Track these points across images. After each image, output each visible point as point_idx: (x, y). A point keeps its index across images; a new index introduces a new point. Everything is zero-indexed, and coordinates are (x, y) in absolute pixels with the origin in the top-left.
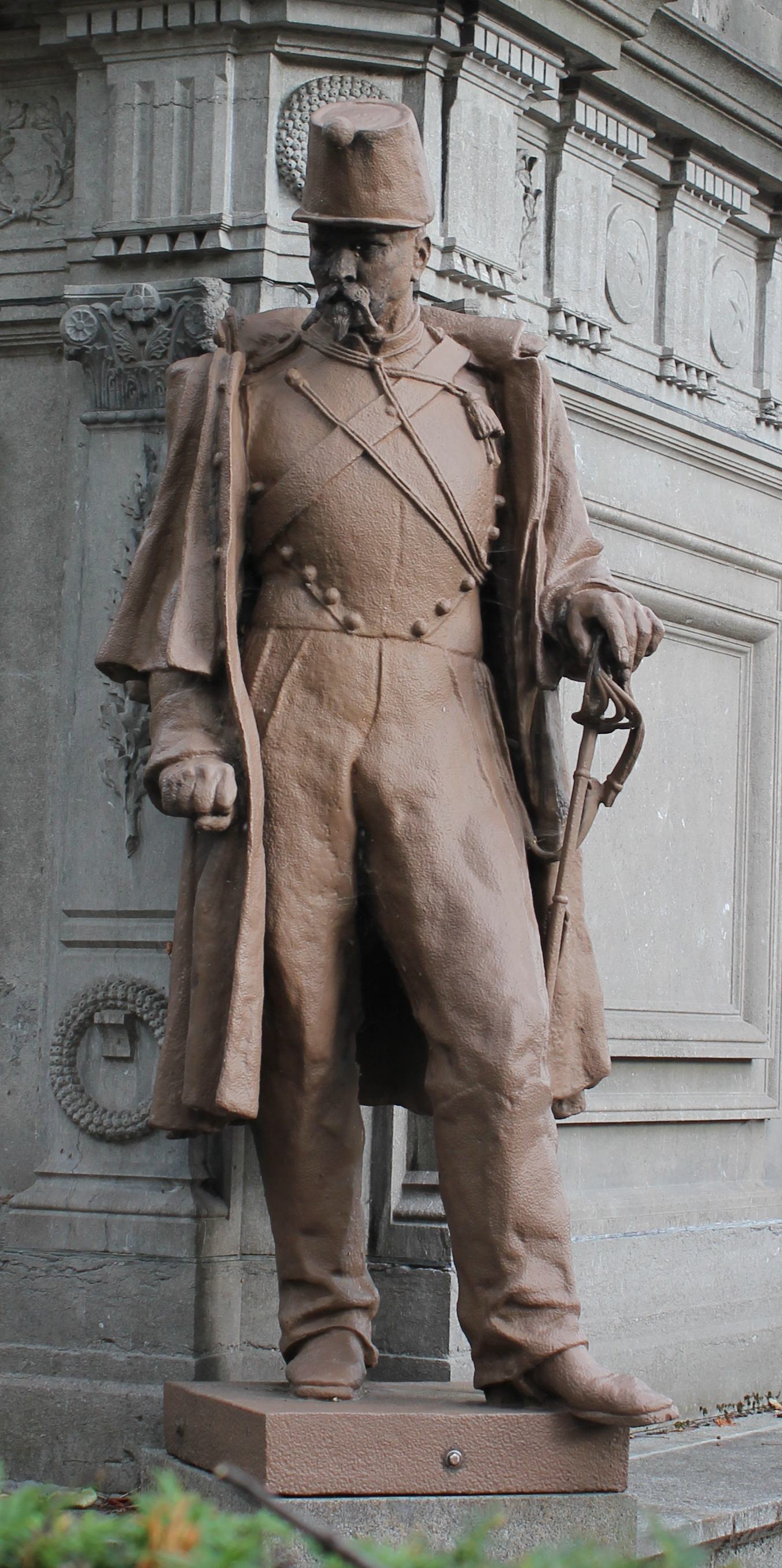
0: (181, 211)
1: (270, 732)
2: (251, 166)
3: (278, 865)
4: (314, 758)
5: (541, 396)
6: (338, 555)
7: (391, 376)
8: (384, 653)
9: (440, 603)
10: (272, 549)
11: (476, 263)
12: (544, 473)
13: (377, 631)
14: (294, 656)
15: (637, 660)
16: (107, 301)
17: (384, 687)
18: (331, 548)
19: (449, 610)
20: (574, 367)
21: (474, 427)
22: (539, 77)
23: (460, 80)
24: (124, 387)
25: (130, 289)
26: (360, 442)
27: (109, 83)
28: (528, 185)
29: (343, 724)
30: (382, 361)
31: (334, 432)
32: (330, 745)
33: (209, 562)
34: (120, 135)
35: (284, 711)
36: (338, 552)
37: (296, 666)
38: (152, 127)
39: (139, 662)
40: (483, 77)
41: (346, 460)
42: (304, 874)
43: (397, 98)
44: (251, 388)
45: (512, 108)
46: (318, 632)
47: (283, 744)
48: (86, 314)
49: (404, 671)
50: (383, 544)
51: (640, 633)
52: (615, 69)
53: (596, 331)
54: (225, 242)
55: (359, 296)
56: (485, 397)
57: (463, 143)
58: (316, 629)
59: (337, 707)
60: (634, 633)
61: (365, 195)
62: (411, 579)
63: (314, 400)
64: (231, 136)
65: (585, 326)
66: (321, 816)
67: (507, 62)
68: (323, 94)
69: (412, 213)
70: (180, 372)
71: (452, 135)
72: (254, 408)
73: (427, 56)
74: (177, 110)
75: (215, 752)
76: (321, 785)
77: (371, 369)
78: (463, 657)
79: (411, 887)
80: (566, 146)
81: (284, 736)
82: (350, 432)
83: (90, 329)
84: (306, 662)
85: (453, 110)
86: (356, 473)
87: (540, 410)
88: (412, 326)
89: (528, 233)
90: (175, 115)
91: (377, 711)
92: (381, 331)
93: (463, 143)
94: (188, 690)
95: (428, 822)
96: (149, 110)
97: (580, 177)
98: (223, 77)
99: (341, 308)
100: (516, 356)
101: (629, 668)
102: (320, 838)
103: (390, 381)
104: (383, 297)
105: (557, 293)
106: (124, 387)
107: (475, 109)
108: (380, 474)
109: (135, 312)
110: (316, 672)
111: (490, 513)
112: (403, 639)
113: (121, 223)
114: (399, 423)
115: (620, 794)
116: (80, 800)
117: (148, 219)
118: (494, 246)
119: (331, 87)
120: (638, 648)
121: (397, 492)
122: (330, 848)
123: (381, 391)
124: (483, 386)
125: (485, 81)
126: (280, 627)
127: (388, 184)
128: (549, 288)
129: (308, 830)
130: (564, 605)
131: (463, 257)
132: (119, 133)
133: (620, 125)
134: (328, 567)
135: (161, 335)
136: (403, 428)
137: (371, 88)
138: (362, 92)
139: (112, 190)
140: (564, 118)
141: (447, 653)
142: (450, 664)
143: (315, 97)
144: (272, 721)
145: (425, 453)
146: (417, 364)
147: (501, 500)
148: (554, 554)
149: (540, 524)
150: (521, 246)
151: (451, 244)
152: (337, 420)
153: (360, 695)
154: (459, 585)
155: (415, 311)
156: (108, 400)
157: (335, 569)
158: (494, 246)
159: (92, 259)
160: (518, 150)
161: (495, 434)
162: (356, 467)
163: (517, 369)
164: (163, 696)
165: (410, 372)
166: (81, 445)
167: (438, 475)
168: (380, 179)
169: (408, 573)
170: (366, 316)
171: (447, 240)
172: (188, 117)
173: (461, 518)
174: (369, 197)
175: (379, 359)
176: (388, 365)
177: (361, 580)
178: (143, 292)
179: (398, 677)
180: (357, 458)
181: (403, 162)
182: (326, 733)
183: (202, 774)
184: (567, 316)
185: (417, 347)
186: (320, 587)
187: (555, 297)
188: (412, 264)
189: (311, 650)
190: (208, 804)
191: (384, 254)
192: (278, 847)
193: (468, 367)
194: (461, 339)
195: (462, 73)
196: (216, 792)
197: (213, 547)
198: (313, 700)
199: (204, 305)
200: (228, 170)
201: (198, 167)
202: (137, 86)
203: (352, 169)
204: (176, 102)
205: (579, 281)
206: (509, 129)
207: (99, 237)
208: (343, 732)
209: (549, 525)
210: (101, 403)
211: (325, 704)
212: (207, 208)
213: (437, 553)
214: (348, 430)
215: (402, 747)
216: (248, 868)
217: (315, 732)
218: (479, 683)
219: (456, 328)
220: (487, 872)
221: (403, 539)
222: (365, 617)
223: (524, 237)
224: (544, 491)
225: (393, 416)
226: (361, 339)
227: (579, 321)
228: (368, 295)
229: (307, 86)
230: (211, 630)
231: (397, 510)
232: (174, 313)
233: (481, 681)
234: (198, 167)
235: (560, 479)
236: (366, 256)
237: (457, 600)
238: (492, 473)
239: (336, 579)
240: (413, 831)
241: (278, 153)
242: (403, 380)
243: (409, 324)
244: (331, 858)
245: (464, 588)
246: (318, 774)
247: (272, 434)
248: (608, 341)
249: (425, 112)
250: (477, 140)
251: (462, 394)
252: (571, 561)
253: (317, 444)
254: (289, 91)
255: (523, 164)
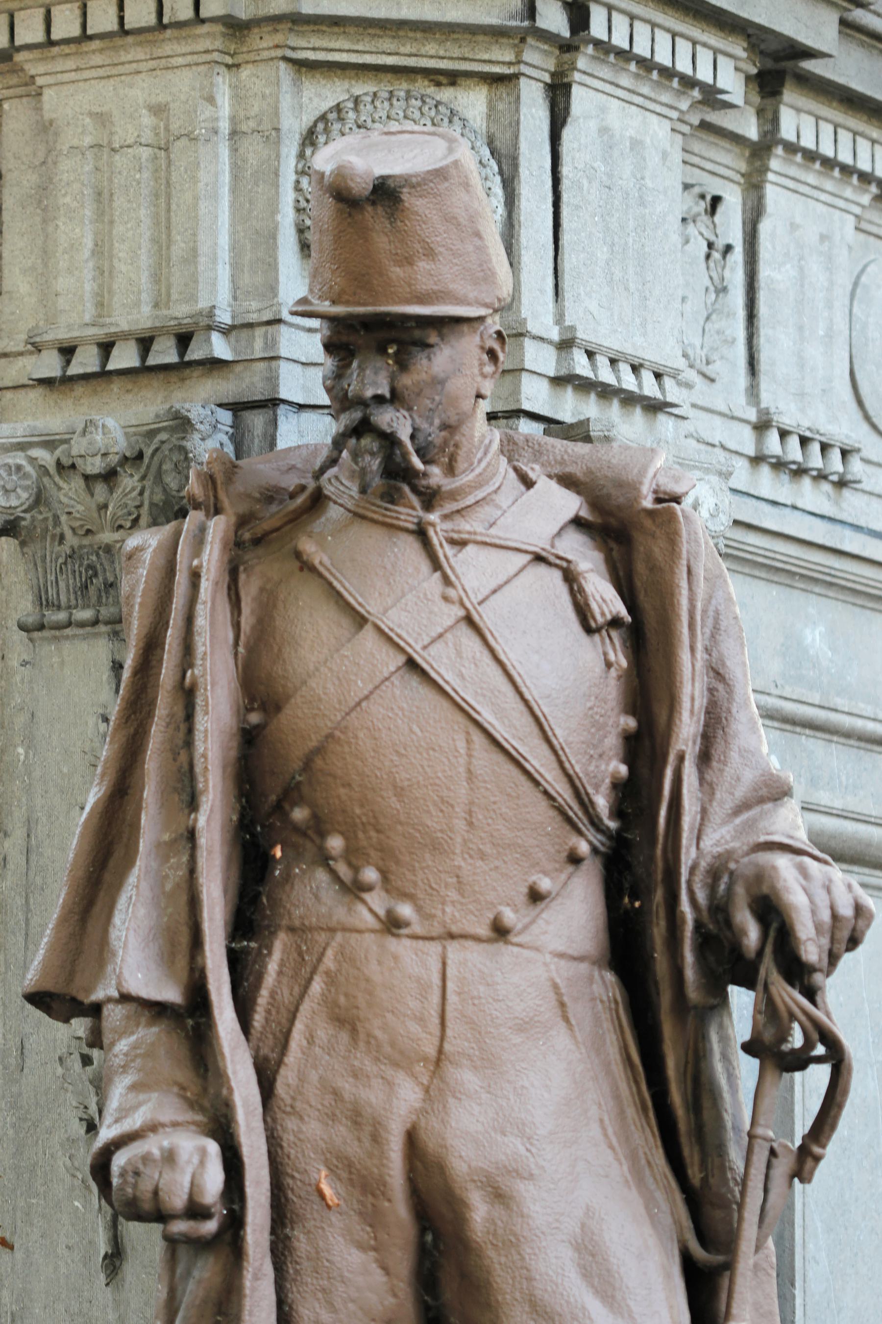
0: (156, 305)
1: (280, 1089)
2: (257, 232)
3: (299, 1292)
4: (347, 1126)
5: (684, 562)
6: (375, 817)
7: (452, 542)
8: (449, 962)
9: (535, 883)
10: (280, 809)
11: (613, 362)
12: (693, 679)
13: (437, 930)
14: (314, 972)
15: (833, 959)
16: (50, 445)
17: (450, 1014)
18: (362, 806)
19: (549, 893)
20: (804, 511)
21: (582, 612)
22: (704, 74)
23: (576, 90)
24: (80, 573)
25: (80, 428)
26: (402, 644)
27: (47, 116)
28: (712, 238)
29: (389, 1072)
30: (438, 521)
31: (364, 631)
32: (371, 1106)
33: (182, 835)
34: (65, 195)
35: (300, 1055)
36: (372, 811)
37: (317, 986)
38: (110, 180)
39: (89, 990)
40: (613, 80)
41: (381, 672)
42: (338, 1303)
43: (478, 119)
44: (245, 570)
45: (667, 125)
46: (347, 935)
47: (299, 1105)
48: (19, 468)
49: (482, 988)
50: (442, 798)
51: (835, 917)
52: (830, 56)
53: (835, 455)
54: (220, 348)
55: (395, 425)
56: (603, 567)
57: (585, 182)
58: (345, 929)
59: (379, 1046)
60: (825, 916)
61: (397, 272)
62: (488, 849)
63: (336, 583)
64: (227, 189)
65: (816, 448)
66: (360, 1214)
67: (649, 57)
68: (363, 118)
69: (472, 295)
70: (139, 549)
71: (565, 170)
72: (249, 599)
73: (519, 54)
74: (145, 153)
75: (194, 1123)
76: (358, 1167)
77: (421, 533)
78: (574, 964)
79: (498, 1317)
80: (771, 176)
81: (301, 1093)
82: (387, 630)
83: (26, 488)
84: (331, 979)
85: (567, 134)
86: (398, 692)
87: (684, 584)
88: (483, 464)
89: (714, 311)
90: (143, 160)
91: (440, 1051)
92: (436, 475)
93: (585, 182)
94: (155, 1029)
95: (522, 1216)
96: (105, 157)
97: (798, 220)
98: (211, 100)
99: (367, 442)
100: (648, 503)
101: (821, 970)
102: (362, 1247)
103: (449, 550)
104: (431, 424)
105: (766, 399)
106: (80, 573)
107: (604, 130)
108: (434, 692)
109: (89, 460)
110: (346, 995)
111: (612, 742)
112: (477, 939)
113: (70, 327)
114: (462, 613)
115: (822, 1164)
116: (34, 1201)
117: (108, 320)
118: (645, 334)
119: (375, 107)
120: (833, 940)
121: (460, 718)
122: (377, 1261)
123: (436, 565)
124: (600, 550)
125: (617, 86)
126: (292, 929)
127: (430, 253)
128: (753, 392)
129: (343, 1236)
130: (725, 879)
131: (590, 354)
132: (63, 192)
133: (859, 139)
134: (361, 835)
135: (130, 492)
136: (469, 620)
137: (436, 106)
138: (422, 113)
139: (55, 278)
140: (764, 134)
141: (548, 957)
142: (554, 974)
143: (350, 123)
144: (283, 1071)
145: (503, 657)
146: (494, 523)
147: (631, 723)
148: (711, 801)
149: (687, 757)
150: (704, 330)
151: (569, 336)
152: (368, 612)
153: (414, 1028)
154: (565, 854)
155: (490, 442)
156: (58, 594)
157: (370, 838)
158: (645, 334)
159: (31, 382)
160: (687, 187)
161: (615, 622)
162: (397, 683)
163: (648, 523)
164: (119, 1039)
165: (481, 534)
166: (24, 664)
167: (524, 689)
168: (417, 246)
169: (481, 838)
170: (405, 455)
171: (565, 329)
172: (163, 163)
173: (561, 753)
174: (402, 275)
175: (433, 517)
176: (448, 525)
177: (411, 853)
178: (100, 430)
179: (472, 998)
180: (399, 669)
181: (450, 219)
182: (364, 1086)
183: (170, 1157)
184: (784, 434)
185: (494, 496)
186: (350, 864)
187: (763, 405)
188: (476, 371)
189: (339, 962)
190: (178, 1201)
191: (430, 359)
192: (297, 1263)
193: (577, 522)
194: (567, 481)
195: (577, 76)
196: (192, 1184)
197: (186, 811)
198: (344, 1037)
199: (188, 445)
200: (224, 240)
201: (179, 238)
202: (88, 120)
203: (374, 235)
204: (143, 141)
205: (803, 379)
206: (665, 155)
207: (38, 348)
208: (390, 1084)
209: (705, 758)
210: (47, 600)
211: (361, 1044)
212: (193, 298)
213: (527, 807)
214: (383, 627)
215: (480, 1104)
216: (245, 1296)
217: (347, 1086)
218: (602, 1001)
219: (561, 464)
220: (614, 1289)
221: (472, 789)
222: (419, 909)
223: (708, 318)
224: (693, 706)
225: (453, 602)
226: (406, 489)
227: (804, 441)
228: (409, 423)
229: (338, 108)
230: (184, 939)
231: (461, 745)
232: (146, 460)
233: (605, 998)
234: (179, 238)
235: (720, 687)
236: (403, 365)
237: (563, 877)
238: (420, 688)
239: (372, 853)
240: (500, 1232)
241: (298, 210)
242: (470, 549)
243: (480, 461)
244: (379, 1277)
245: (574, 859)
246: (354, 1150)
247: (274, 638)
248: (856, 467)
249: (522, 138)
250: (610, 176)
251: (565, 564)
252: (738, 811)
253: (338, 650)
254: (313, 119)
255: (703, 205)
